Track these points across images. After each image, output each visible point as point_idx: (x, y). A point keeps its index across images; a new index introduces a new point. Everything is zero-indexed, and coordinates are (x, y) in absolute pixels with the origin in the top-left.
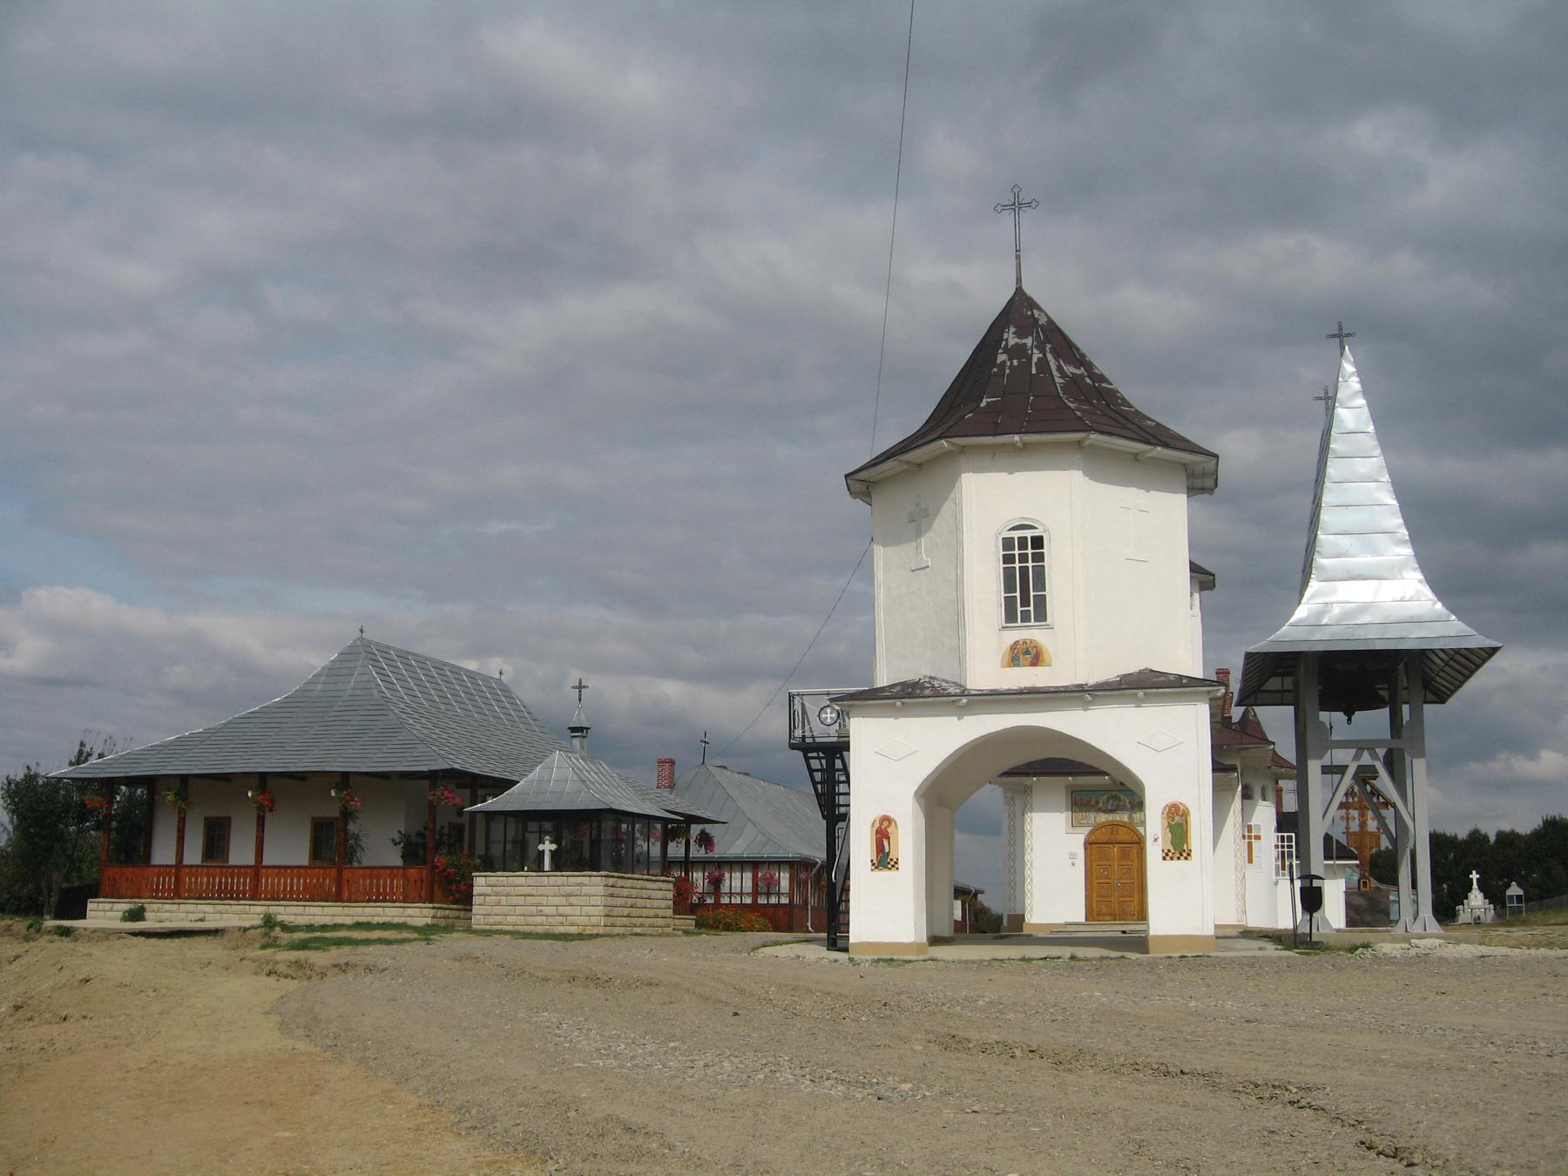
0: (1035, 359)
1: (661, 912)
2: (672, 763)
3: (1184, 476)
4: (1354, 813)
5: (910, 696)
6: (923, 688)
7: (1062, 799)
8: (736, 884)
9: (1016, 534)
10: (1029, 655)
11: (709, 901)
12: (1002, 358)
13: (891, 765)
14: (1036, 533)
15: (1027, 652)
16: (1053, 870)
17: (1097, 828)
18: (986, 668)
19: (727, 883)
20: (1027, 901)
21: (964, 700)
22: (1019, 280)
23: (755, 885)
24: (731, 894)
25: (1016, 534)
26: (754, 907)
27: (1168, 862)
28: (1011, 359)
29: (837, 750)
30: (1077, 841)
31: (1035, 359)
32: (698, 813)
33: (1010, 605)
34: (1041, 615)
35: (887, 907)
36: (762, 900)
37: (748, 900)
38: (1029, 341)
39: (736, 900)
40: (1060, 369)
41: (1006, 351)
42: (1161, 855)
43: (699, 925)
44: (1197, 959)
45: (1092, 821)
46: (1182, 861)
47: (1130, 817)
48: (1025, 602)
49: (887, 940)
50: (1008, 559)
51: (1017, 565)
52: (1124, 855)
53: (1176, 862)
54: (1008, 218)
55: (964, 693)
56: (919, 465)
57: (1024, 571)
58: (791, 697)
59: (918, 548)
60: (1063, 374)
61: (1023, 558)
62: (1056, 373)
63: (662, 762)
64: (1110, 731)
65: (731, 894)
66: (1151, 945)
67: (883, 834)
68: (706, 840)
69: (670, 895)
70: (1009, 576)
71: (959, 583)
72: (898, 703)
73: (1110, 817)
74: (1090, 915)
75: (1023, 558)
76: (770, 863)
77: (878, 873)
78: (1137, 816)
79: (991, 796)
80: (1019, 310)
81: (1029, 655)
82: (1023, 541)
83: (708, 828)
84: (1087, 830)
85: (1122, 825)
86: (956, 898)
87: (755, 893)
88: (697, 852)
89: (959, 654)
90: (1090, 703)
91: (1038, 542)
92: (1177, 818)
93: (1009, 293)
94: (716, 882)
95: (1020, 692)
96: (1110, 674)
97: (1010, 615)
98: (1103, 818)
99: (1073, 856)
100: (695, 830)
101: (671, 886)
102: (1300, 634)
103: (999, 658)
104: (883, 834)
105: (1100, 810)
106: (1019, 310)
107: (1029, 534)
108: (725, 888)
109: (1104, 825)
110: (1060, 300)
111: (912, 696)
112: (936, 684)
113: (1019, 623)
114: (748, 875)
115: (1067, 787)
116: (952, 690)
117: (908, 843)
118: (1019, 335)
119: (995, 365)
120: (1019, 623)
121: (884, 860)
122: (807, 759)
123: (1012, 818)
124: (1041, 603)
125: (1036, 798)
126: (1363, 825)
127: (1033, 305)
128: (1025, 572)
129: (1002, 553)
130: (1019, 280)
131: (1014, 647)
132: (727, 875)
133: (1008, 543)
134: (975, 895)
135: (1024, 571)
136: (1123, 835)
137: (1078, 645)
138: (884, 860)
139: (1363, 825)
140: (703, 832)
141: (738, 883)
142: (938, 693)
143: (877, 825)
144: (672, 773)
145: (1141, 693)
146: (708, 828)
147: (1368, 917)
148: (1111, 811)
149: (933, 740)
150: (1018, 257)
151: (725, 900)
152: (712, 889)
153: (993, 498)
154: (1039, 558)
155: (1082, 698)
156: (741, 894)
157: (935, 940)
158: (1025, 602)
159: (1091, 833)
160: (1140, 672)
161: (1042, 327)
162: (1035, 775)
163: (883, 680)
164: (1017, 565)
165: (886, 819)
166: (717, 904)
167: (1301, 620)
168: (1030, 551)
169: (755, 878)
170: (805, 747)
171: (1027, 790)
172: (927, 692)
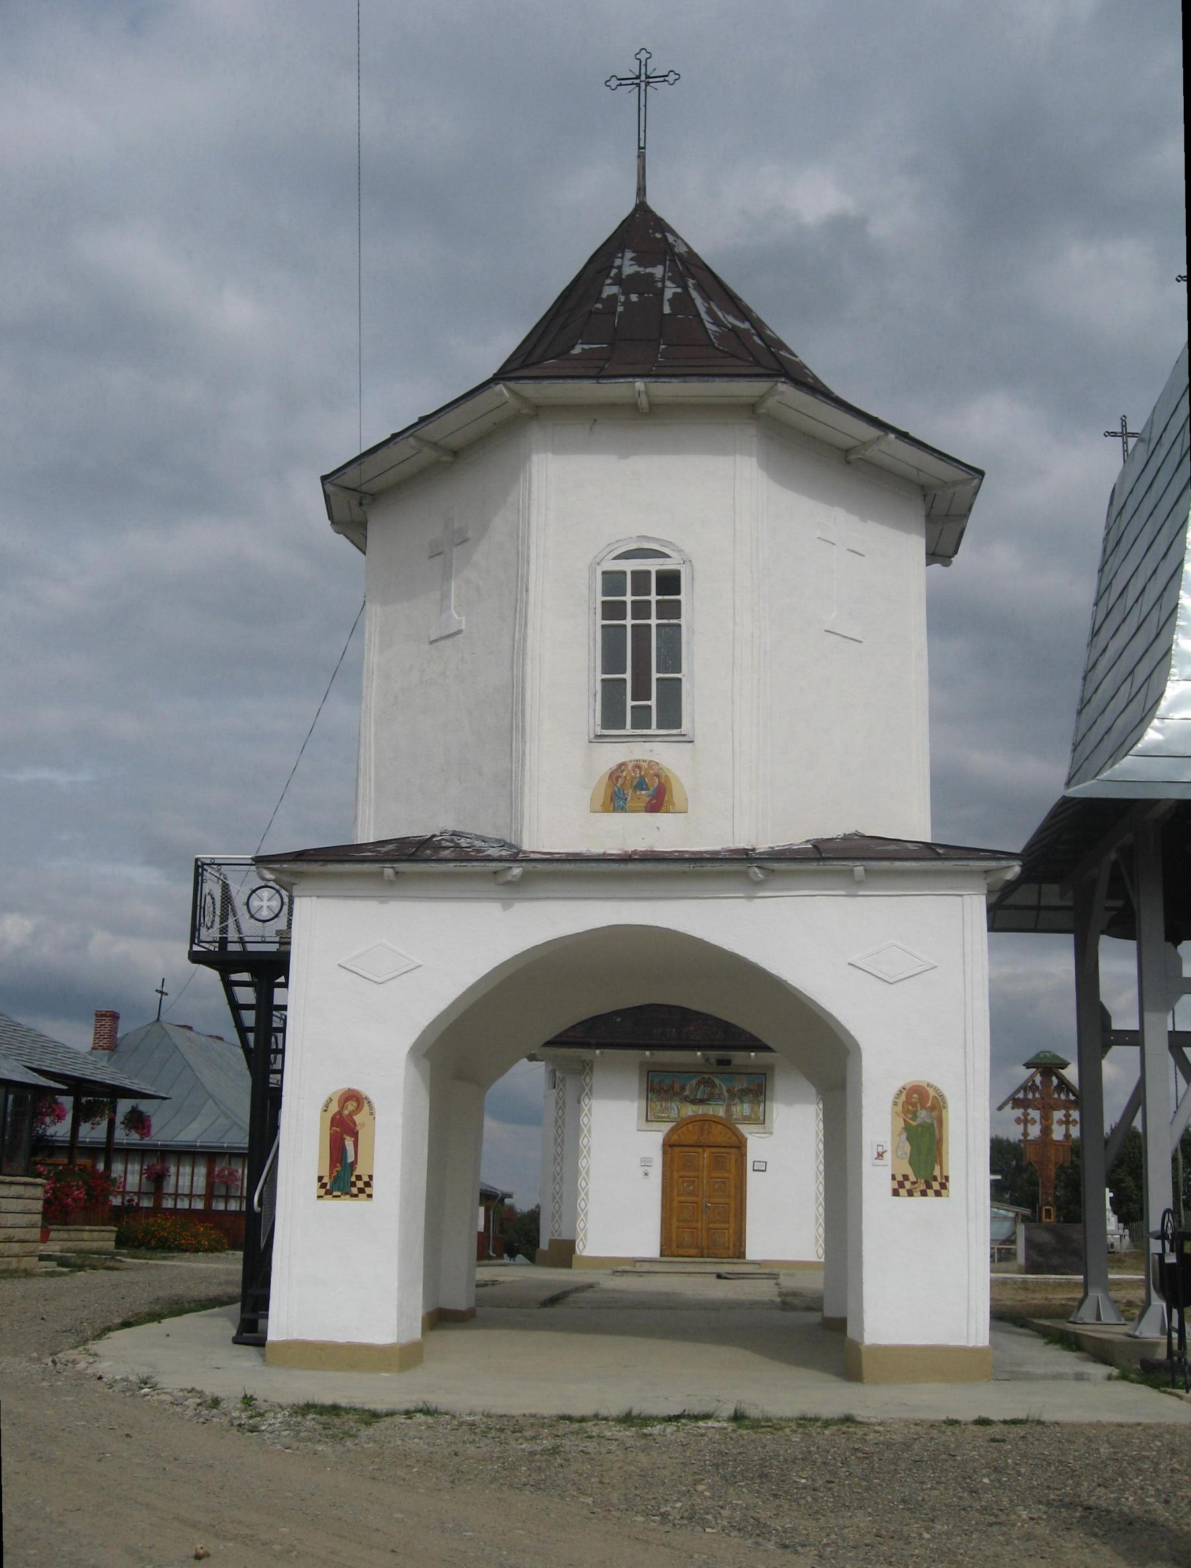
0: (668, 294)
1: (19, 1234)
2: (115, 1017)
3: (918, 513)
4: (1034, 1114)
5: (412, 858)
6: (439, 847)
7: (634, 1082)
8: (184, 1182)
9: (629, 566)
10: (646, 791)
11: (146, 1203)
12: (609, 290)
13: (369, 993)
14: (668, 565)
15: (641, 785)
16: (614, 1180)
17: (681, 1125)
18: (560, 812)
19: (172, 1180)
20: (580, 1225)
21: (517, 871)
22: (641, 190)
23: (210, 1185)
24: (176, 1196)
25: (629, 566)
26: (207, 1215)
27: (904, 1201)
28: (626, 293)
29: (271, 968)
30: (652, 1142)
31: (668, 294)
32: (127, 1083)
33: (611, 694)
34: (671, 715)
35: (345, 1271)
36: (220, 1206)
37: (199, 1205)
38: (658, 271)
39: (183, 1204)
40: (710, 312)
41: (618, 280)
42: (889, 1185)
43: (121, 1242)
44: (258, 998)
45: (674, 1114)
46: (931, 1199)
47: (728, 1111)
48: (641, 691)
49: (341, 1338)
50: (612, 610)
51: (629, 622)
52: (718, 1163)
53: (917, 1200)
54: (628, 96)
55: (517, 856)
56: (455, 453)
57: (641, 633)
58: (199, 868)
59: (445, 596)
60: (717, 322)
61: (641, 610)
62: (705, 316)
63: (100, 1016)
64: (795, 940)
65: (176, 1196)
66: (867, 1365)
67: (345, 1124)
68: (138, 1121)
69: (39, 1205)
70: (612, 641)
71: (517, 653)
72: (388, 871)
73: (700, 1110)
74: (669, 1246)
75: (641, 610)
76: (232, 1155)
77: (330, 1204)
78: (743, 1109)
79: (528, 1077)
80: (643, 231)
81: (646, 791)
82: (641, 578)
83: (144, 1106)
84: (667, 1127)
85: (716, 1121)
86: (481, 1204)
87: (209, 1196)
88: (122, 1136)
89: (510, 788)
90: (758, 884)
91: (670, 582)
92: (923, 1114)
93: (627, 206)
94: (157, 1179)
95: (627, 858)
96: (797, 836)
97: (612, 716)
98: (690, 1110)
99: (646, 1163)
100: (124, 1106)
101: (39, 1192)
102: (1157, 770)
103: (588, 794)
104: (345, 1124)
105: (686, 1099)
106: (643, 231)
107: (653, 566)
108: (169, 1186)
109: (692, 1120)
110: (703, 221)
111: (413, 861)
112: (463, 842)
113: (628, 730)
114: (201, 1170)
115: (642, 1064)
116: (494, 852)
117: (393, 1148)
118: (638, 261)
119: (598, 299)
120: (628, 730)
121: (343, 1178)
122: (229, 986)
123: (561, 1105)
124: (672, 694)
125: (598, 1079)
126: (1046, 1130)
127: (661, 225)
128: (643, 640)
129: (600, 598)
130: (641, 190)
131: (615, 775)
132: (173, 1169)
133: (613, 582)
134: (502, 1200)
135: (641, 633)
136: (718, 1135)
137: (741, 772)
138: (343, 1178)
139: (1046, 1130)
140: (134, 1111)
141: (188, 1181)
142: (464, 856)
143: (334, 1108)
144: (114, 1030)
145: (859, 868)
146: (144, 1106)
147: (1056, 1261)
148: (702, 1102)
149: (461, 944)
150: (642, 157)
151: (168, 1204)
152: (148, 1187)
153: (588, 501)
154: (671, 610)
155: (744, 875)
156: (190, 1196)
157: (440, 1319)
158: (641, 691)
159: (673, 1130)
160: (846, 838)
161: (680, 256)
162: (599, 1046)
163: (367, 833)
164: (629, 622)
165: (353, 1098)
166: (157, 1209)
167: (1157, 745)
168: (653, 597)
169: (210, 1175)
170: (222, 960)
171: (585, 1068)
172: (445, 854)
